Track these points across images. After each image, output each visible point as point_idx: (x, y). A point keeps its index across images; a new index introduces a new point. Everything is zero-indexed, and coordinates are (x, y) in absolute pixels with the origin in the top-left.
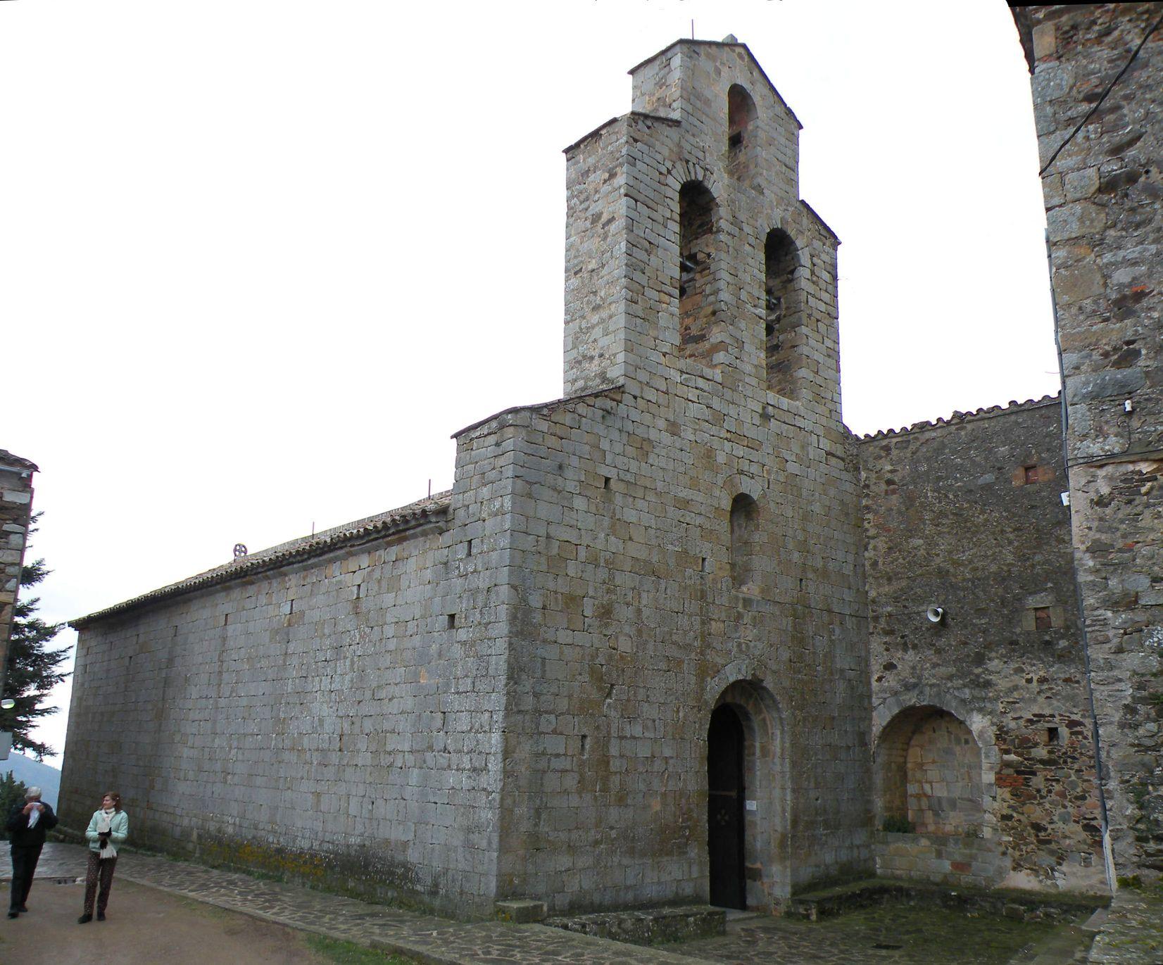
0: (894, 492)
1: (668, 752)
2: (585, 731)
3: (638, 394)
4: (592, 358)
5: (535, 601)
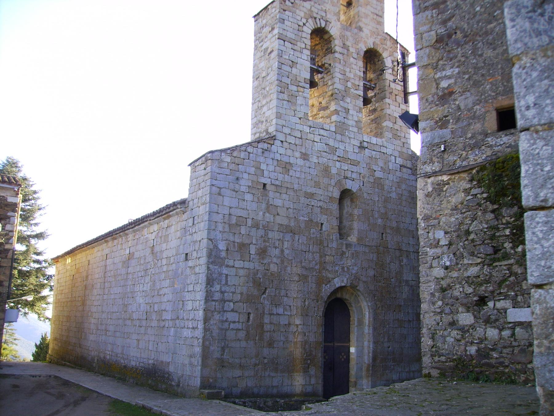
2: (250, 311)
3: (283, 140)
4: (263, 122)
5: (222, 246)
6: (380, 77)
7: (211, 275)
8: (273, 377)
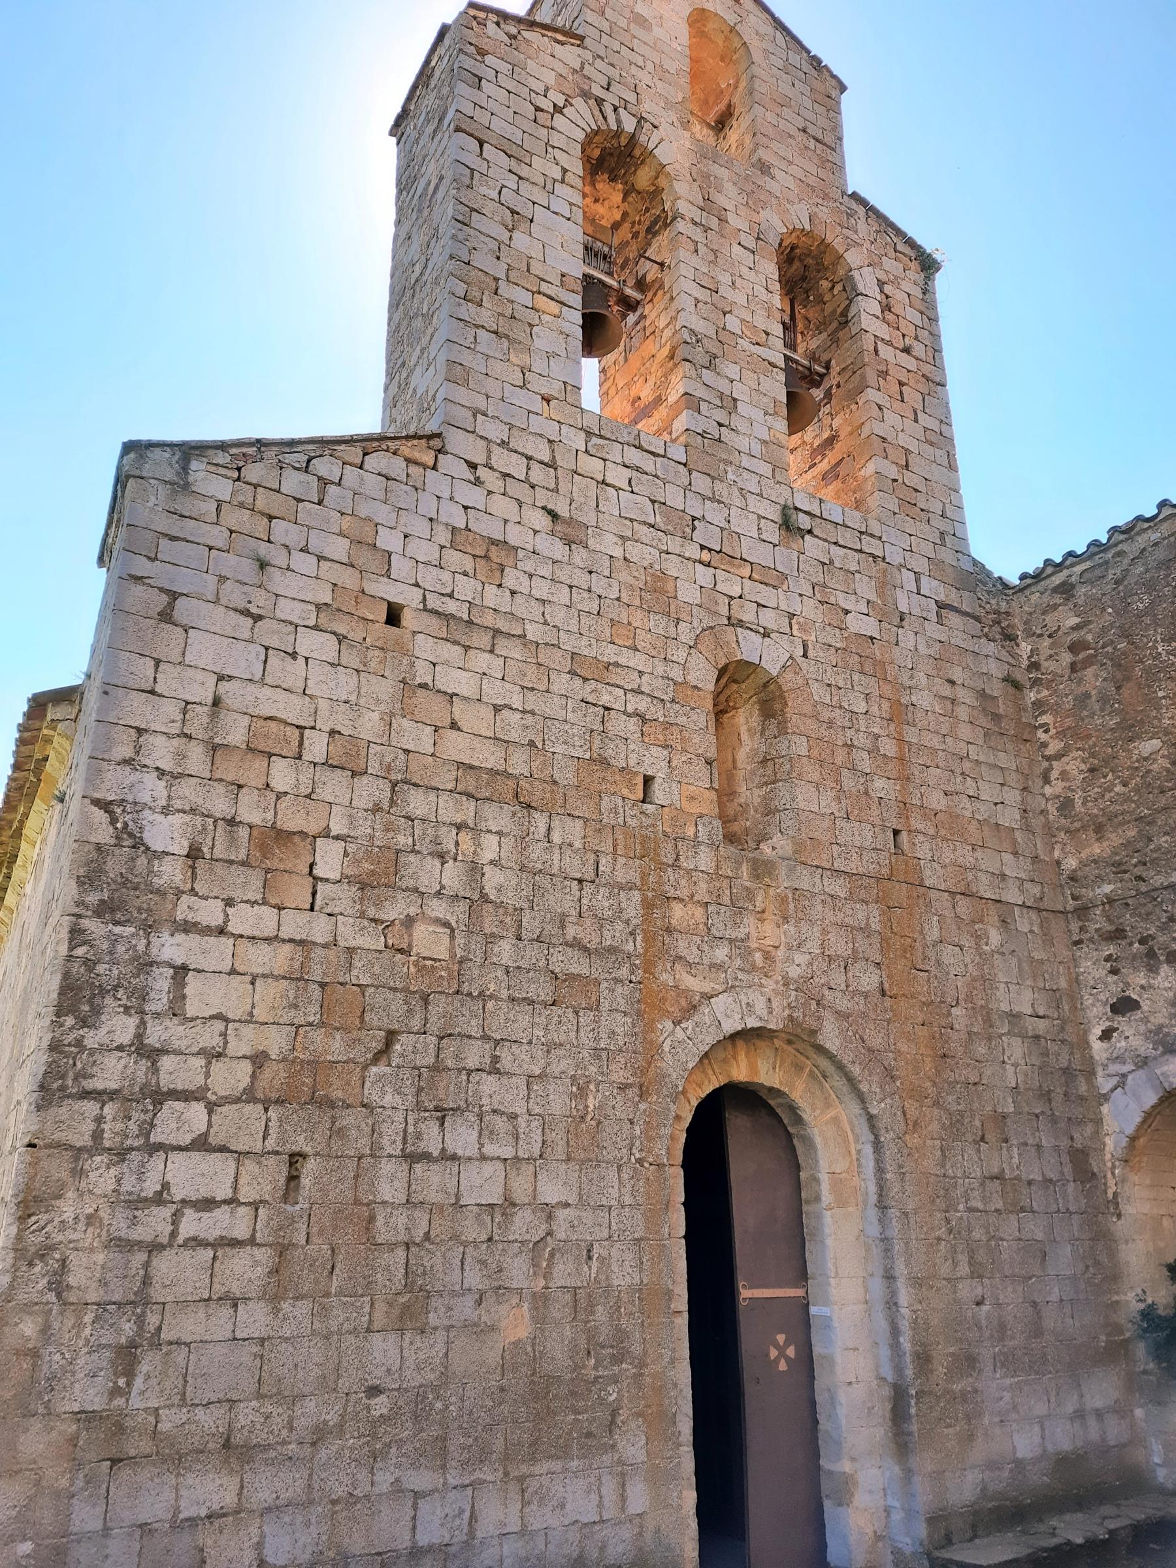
0: (1088, 662)
1: (551, 1193)
2: (301, 1143)
5: (166, 834)
6: (841, 334)
7: (90, 964)
8: (417, 1495)
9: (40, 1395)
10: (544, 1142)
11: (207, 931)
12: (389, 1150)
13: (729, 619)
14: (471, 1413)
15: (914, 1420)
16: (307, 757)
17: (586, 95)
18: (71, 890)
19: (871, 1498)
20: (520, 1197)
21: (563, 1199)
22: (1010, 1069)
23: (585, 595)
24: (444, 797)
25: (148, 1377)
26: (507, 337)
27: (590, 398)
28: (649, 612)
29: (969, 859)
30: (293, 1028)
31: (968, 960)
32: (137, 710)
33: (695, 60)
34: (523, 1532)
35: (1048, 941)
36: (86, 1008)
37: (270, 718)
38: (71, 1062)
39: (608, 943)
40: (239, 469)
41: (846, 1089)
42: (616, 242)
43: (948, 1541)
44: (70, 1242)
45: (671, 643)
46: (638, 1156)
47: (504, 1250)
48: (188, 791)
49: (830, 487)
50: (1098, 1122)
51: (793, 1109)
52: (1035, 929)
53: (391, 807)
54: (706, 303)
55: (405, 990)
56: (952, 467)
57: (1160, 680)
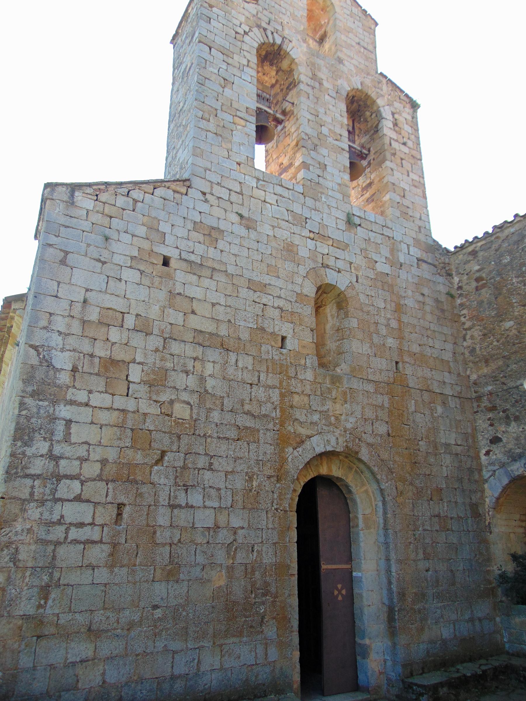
0: (484, 286)
1: (236, 522)
2: (122, 499)
5: (63, 361)
6: (375, 136)
7: (28, 418)
8: (174, 652)
9: (5, 608)
10: (233, 500)
11: (80, 404)
12: (162, 503)
13: (322, 264)
14: (199, 617)
15: (397, 622)
16: (125, 326)
17: (259, 26)
18: (20, 385)
19: (378, 658)
20: (222, 524)
21: (241, 525)
22: (444, 468)
23: (256, 252)
24: (188, 346)
25: (54, 600)
26: (221, 136)
27: (260, 163)
28: (285, 260)
29: (429, 374)
30: (119, 449)
31: (427, 420)
32: (49, 304)
33: (310, 11)
34: (221, 669)
35: (463, 411)
36: (26, 438)
37: (109, 309)
38: (20, 461)
39: (264, 413)
40: (97, 195)
41: (371, 477)
42: (273, 92)
43: (412, 675)
44: (20, 540)
45: (296, 275)
46: (275, 507)
47: (214, 547)
48: (71, 341)
49: (370, 205)
50: (483, 491)
51: (347, 486)
52: (458, 406)
53: (164, 350)
54: (313, 121)
55: (170, 433)
56: (425, 197)
57: (514, 295)
